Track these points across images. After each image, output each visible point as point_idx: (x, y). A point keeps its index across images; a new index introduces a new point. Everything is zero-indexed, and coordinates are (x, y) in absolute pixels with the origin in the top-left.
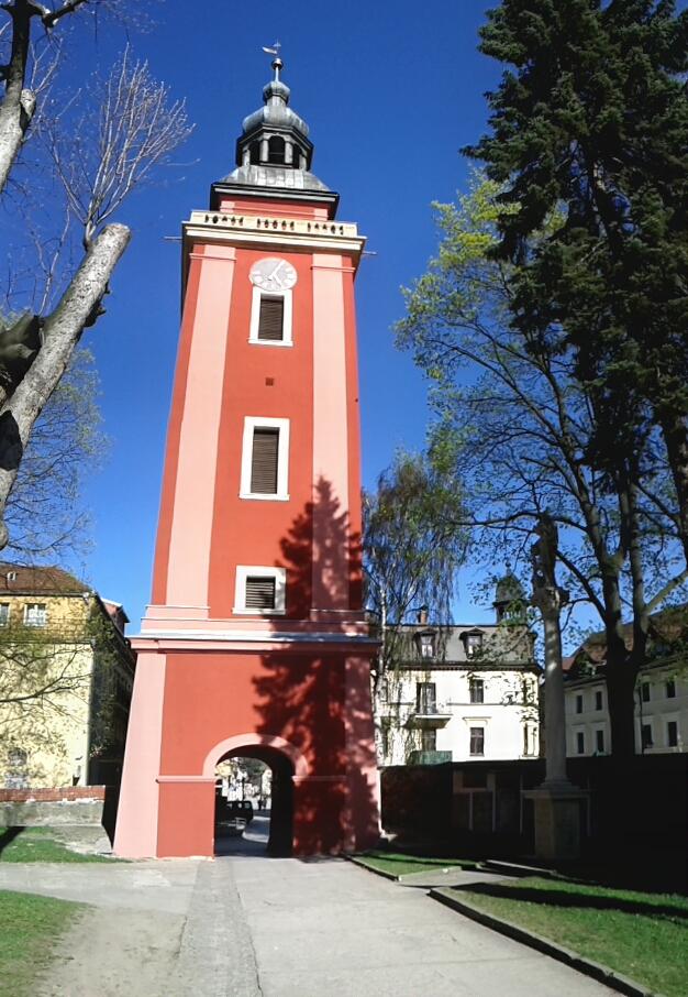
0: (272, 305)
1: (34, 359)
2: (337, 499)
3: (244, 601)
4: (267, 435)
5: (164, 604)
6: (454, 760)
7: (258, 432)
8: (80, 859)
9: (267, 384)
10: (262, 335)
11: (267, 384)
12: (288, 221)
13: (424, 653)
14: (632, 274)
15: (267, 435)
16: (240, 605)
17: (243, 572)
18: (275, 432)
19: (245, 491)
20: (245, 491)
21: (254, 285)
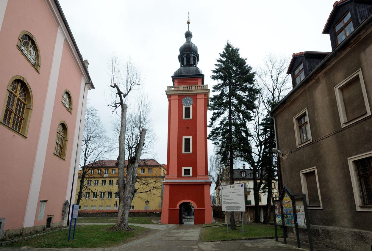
0: (187, 109)
1: (147, 178)
2: (254, 73)
3: (184, 174)
4: (187, 140)
5: (169, 175)
6: (259, 203)
7: (185, 139)
8: (155, 224)
9: (188, 127)
10: (185, 117)
11: (188, 127)
12: (190, 86)
13: (243, 176)
14: (269, 145)
15: (187, 140)
16: (183, 175)
17: (184, 168)
18: (189, 139)
19: (183, 152)
20: (183, 152)
21: (183, 105)
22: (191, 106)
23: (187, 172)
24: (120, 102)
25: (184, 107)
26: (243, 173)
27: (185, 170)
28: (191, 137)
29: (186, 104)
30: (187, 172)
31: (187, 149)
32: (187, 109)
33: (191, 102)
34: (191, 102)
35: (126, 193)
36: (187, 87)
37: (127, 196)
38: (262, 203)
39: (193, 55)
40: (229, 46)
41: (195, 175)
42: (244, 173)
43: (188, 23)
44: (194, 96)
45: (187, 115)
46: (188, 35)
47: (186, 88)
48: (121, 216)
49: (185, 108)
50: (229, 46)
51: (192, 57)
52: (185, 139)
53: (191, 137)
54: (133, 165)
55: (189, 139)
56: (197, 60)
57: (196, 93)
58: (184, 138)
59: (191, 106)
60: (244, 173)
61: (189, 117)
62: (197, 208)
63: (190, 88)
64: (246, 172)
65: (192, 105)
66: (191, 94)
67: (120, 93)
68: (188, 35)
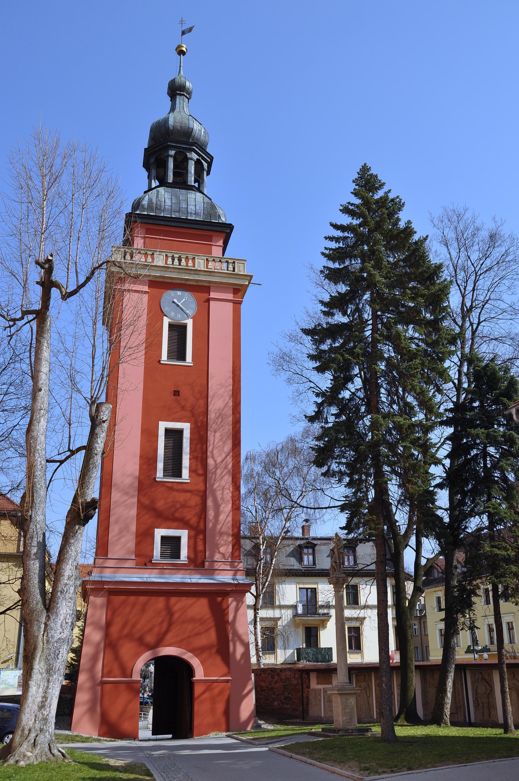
0: (178, 331)
7: (168, 431)
18: (180, 432)
19: (160, 474)
22: (190, 323)
23: (171, 545)
24: (37, 307)
25: (166, 321)
26: (305, 551)
27: (163, 538)
28: (161, 423)
30: (171, 545)
32: (178, 331)
34: (192, 308)
35: (52, 625)
36: (180, 260)
37: (57, 636)
38: (362, 657)
39: (195, 156)
40: (365, 164)
41: (198, 562)
42: (310, 551)
44: (201, 289)
45: (178, 351)
47: (176, 261)
48: (36, 708)
49: (170, 326)
50: (365, 164)
51: (193, 162)
52: (168, 431)
53: (161, 423)
54: (82, 528)
55: (180, 432)
56: (205, 173)
57: (210, 282)
58: (163, 426)
59: (190, 323)
60: (310, 551)
62: (204, 678)
63: (190, 263)
64: (317, 548)
65: (194, 318)
66: (191, 283)
67: (47, 285)
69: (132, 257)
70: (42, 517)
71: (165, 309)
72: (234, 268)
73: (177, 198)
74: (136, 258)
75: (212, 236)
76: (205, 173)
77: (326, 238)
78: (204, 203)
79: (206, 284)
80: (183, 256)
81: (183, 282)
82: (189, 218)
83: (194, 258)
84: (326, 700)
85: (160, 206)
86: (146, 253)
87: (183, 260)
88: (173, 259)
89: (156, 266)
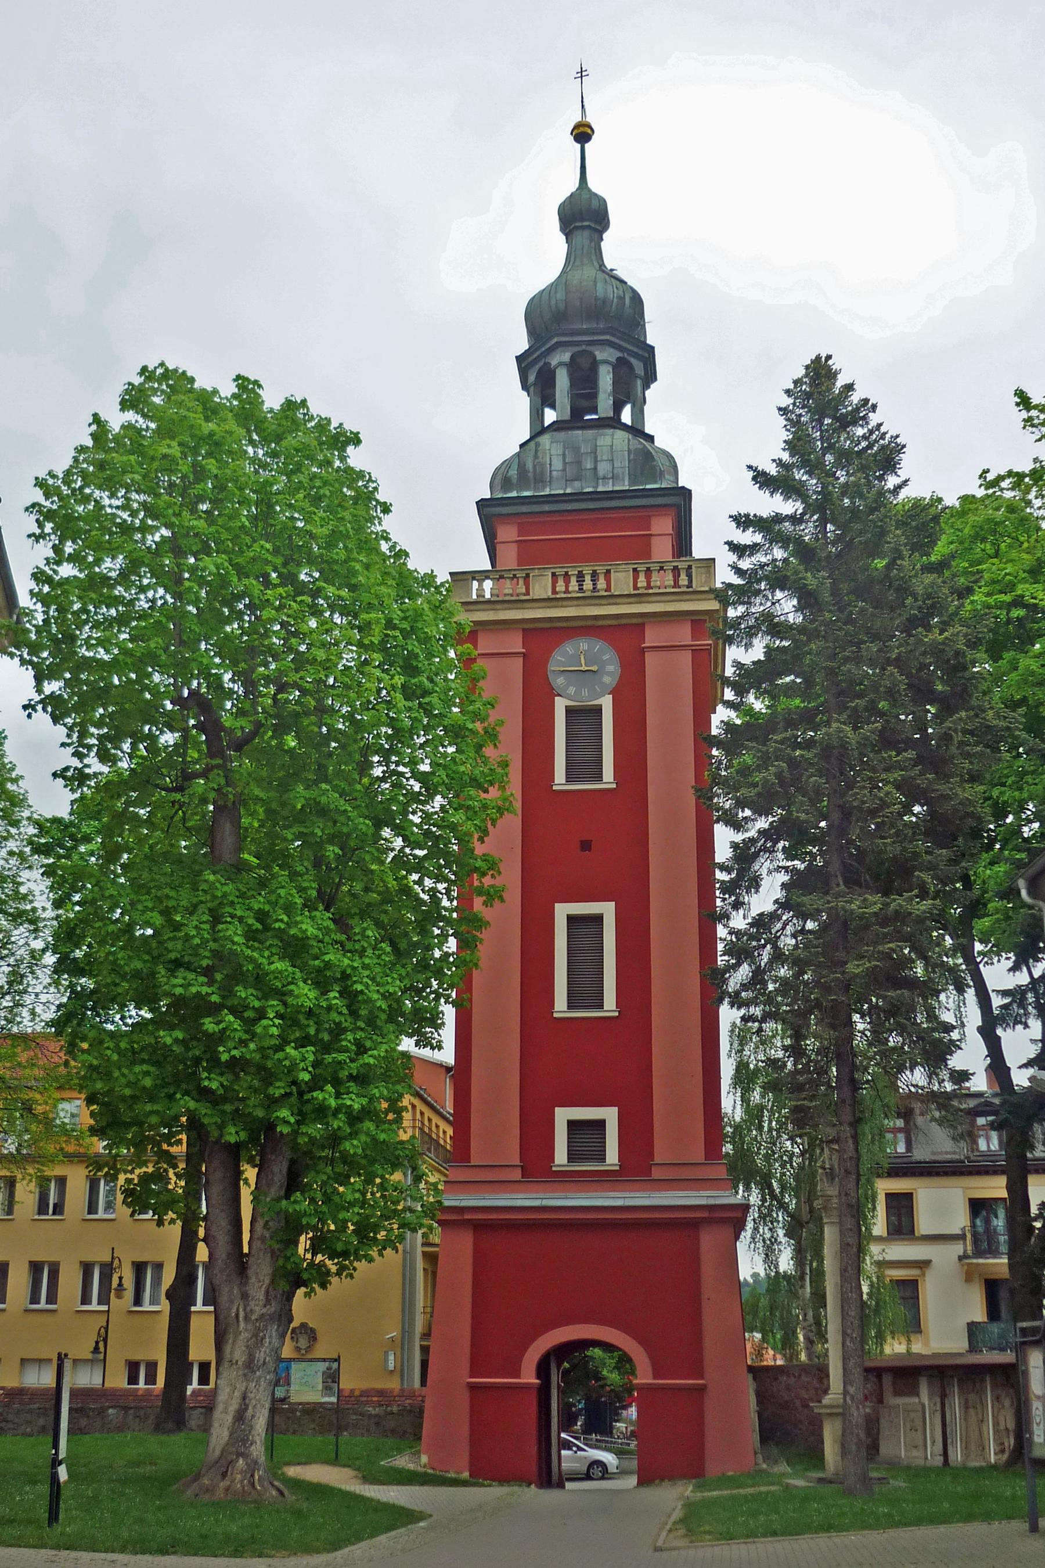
0: (583, 718)
4: (584, 927)
15: (584, 927)
18: (597, 920)
25: (560, 705)
28: (558, 906)
29: (572, 690)
31: (583, 765)
32: (583, 718)
33: (611, 670)
41: (637, 1165)
43: (582, 134)
44: (626, 635)
46: (584, 218)
49: (569, 711)
53: (558, 906)
59: (606, 703)
61: (598, 777)
63: (602, 584)
65: (616, 693)
68: (584, 218)
69: (648, 578)
70: (852, 1390)
71: (559, 682)
72: (690, 581)
73: (576, 450)
74: (656, 578)
75: (649, 517)
76: (639, 382)
77: (907, 481)
78: (629, 451)
79: (634, 621)
80: (587, 571)
81: (589, 623)
82: (600, 489)
83: (608, 572)
84: (908, 1427)
85: (542, 473)
86: (648, 569)
87: (588, 578)
88: (567, 582)
89: (533, 600)
